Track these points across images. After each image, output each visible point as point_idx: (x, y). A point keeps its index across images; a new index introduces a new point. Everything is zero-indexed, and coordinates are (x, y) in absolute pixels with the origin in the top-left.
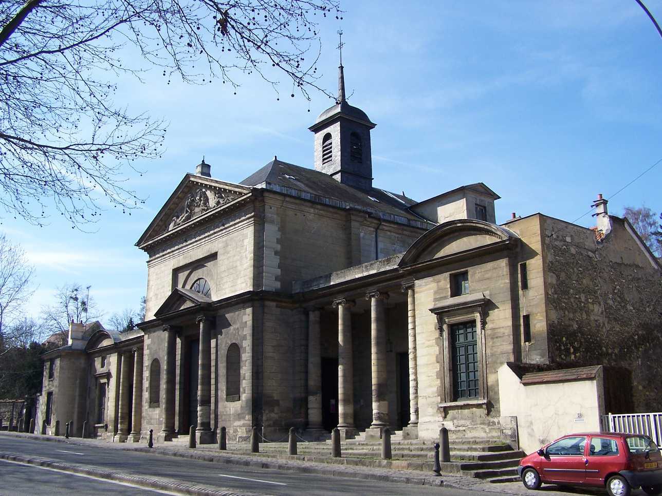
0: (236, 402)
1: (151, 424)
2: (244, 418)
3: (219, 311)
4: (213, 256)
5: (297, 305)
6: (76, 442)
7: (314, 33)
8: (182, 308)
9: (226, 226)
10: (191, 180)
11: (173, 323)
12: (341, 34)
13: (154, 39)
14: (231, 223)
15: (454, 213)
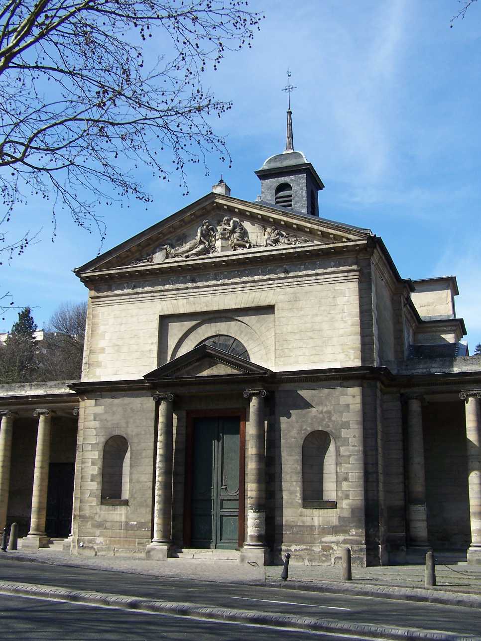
0: (329, 509)
1: (105, 528)
2: (346, 532)
3: (282, 385)
4: (269, 309)
5: (395, 389)
6: (45, 559)
7: (202, 62)
8: (205, 373)
9: (291, 274)
10: (214, 202)
11: (181, 391)
12: (289, 76)
13: (217, 2)
14: (305, 273)
15: (434, 303)
